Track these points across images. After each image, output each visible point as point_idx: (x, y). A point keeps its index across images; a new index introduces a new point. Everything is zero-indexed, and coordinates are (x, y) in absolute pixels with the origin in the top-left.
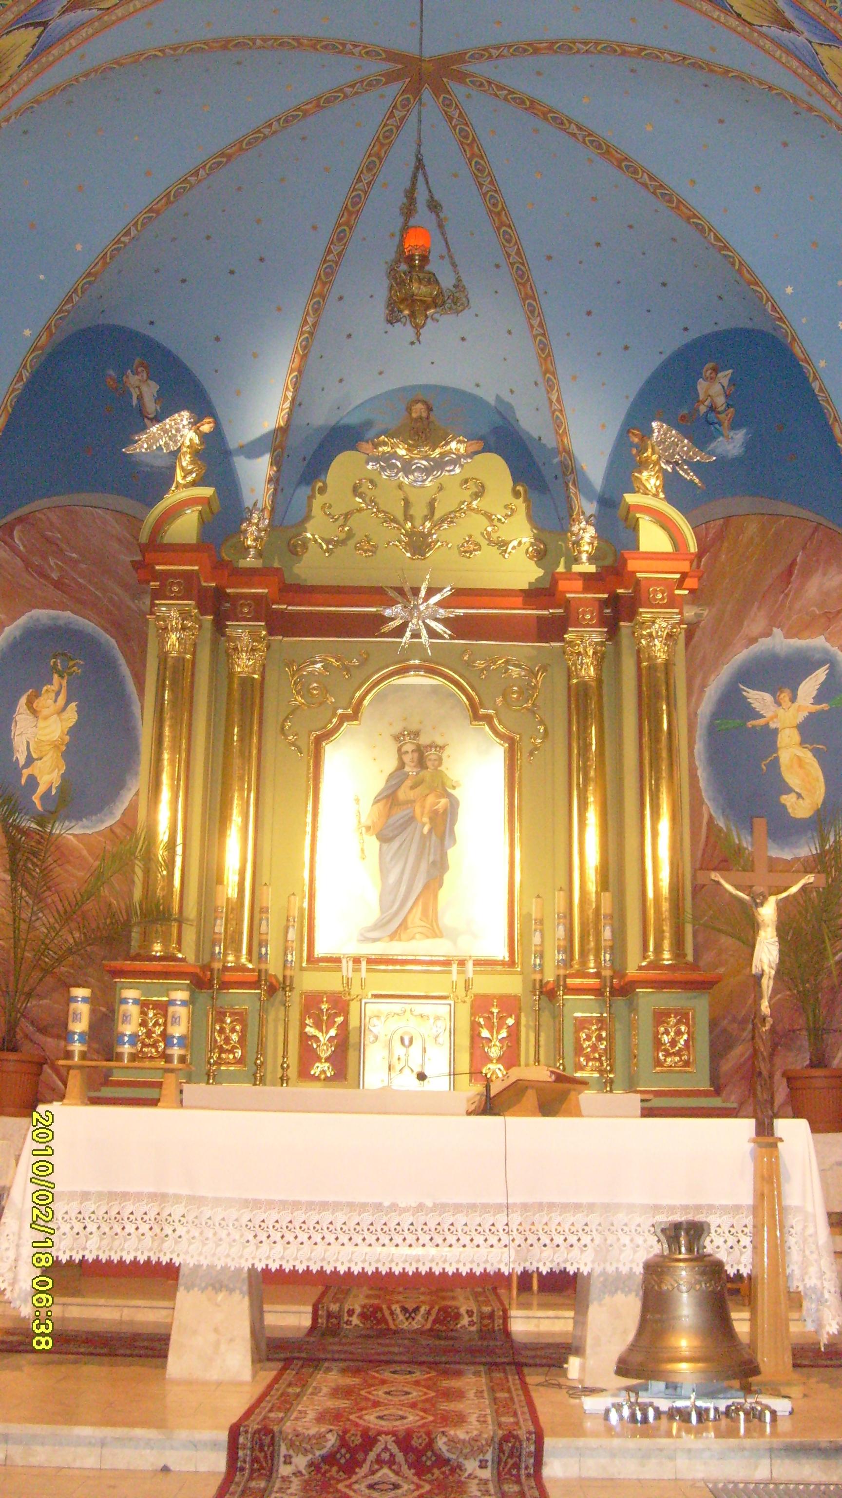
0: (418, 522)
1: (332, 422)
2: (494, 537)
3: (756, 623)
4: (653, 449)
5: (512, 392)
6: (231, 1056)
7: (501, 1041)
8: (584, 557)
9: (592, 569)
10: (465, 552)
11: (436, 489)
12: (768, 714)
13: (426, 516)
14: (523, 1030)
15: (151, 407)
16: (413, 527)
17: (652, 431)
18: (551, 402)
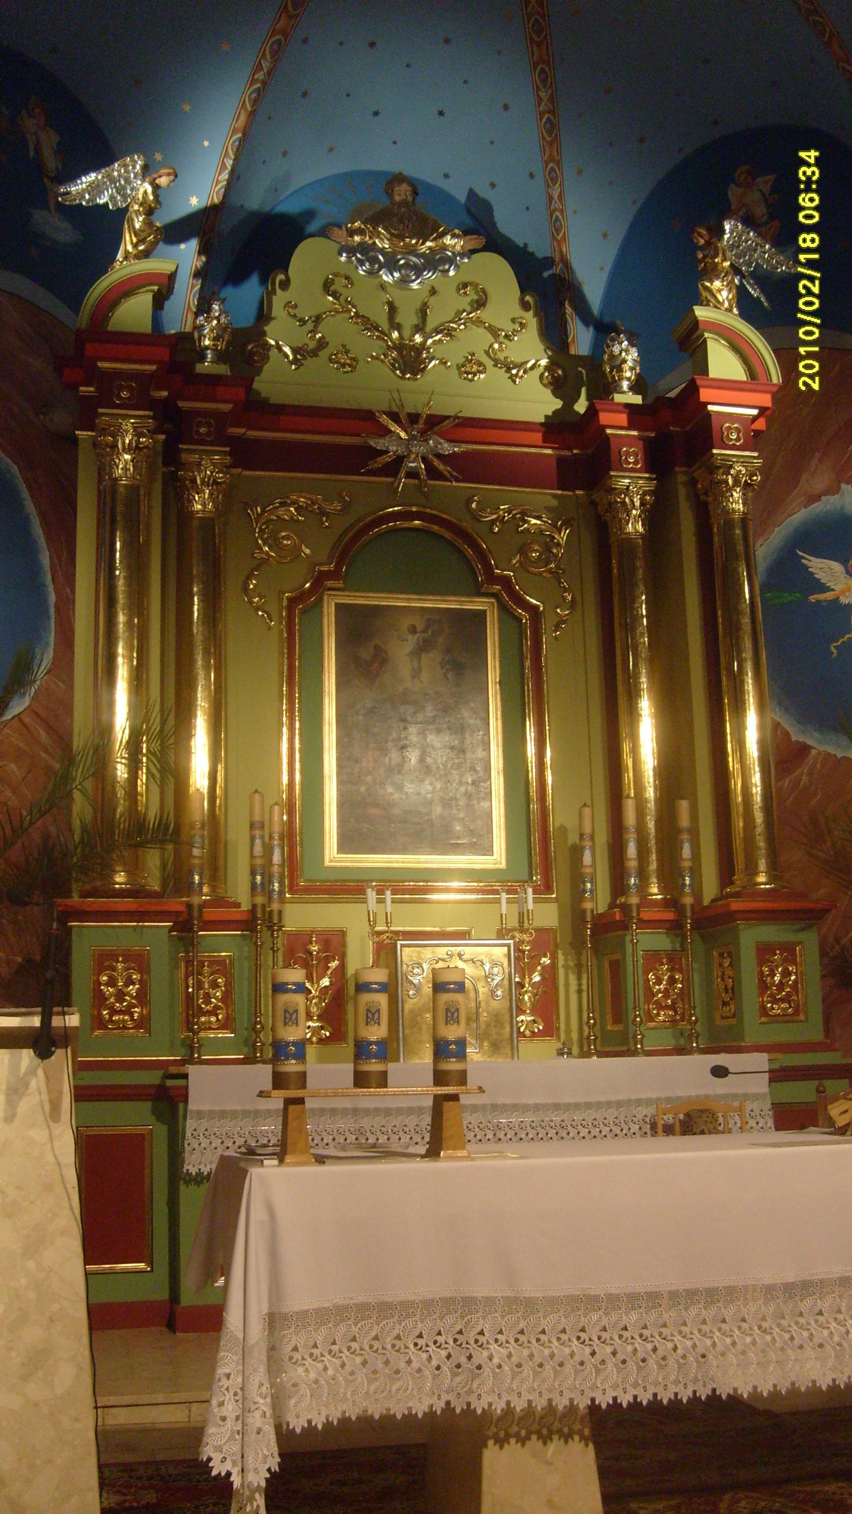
0: (407, 333)
1: (267, 208)
2: (501, 356)
3: (818, 478)
4: (724, 254)
5: (493, 185)
6: (213, 1019)
7: (533, 985)
8: (625, 385)
9: (637, 400)
10: (468, 373)
11: (426, 293)
12: (838, 588)
13: (417, 326)
14: (561, 972)
15: (51, 162)
16: (401, 337)
17: (723, 232)
18: (551, 198)
